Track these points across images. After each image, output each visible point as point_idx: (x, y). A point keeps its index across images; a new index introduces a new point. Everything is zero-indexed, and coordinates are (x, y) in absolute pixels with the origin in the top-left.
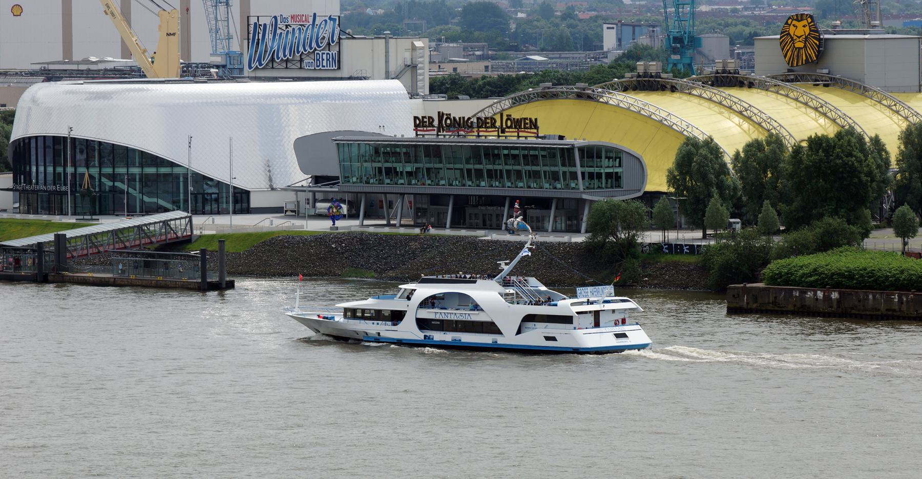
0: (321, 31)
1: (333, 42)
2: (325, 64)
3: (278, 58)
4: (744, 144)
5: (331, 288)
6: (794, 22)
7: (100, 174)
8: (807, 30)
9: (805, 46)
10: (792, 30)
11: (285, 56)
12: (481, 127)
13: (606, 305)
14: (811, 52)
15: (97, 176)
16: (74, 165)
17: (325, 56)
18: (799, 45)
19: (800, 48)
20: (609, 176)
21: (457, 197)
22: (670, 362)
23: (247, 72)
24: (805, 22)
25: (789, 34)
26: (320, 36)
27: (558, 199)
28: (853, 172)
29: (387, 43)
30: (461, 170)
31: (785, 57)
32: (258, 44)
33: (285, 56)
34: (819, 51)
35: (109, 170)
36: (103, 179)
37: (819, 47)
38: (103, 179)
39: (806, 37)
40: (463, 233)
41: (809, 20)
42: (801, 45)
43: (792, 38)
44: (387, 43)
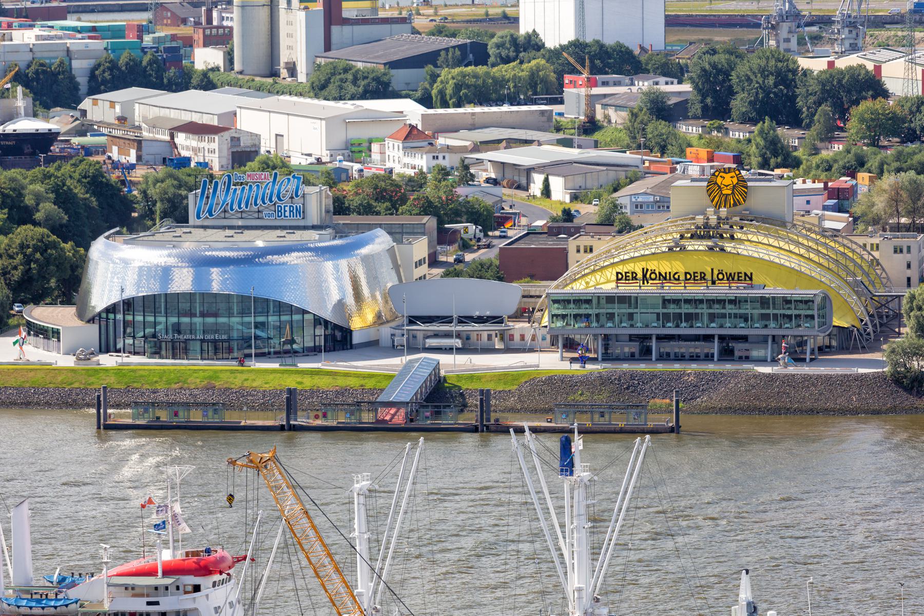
0: (283, 187)
1: (297, 196)
2: (287, 214)
3: (232, 209)
5: (143, 440)
6: (722, 174)
8: (735, 180)
9: (733, 193)
10: (719, 180)
11: (240, 207)
17: (287, 209)
18: (726, 191)
19: (727, 195)
20: (807, 316)
22: (643, 463)
23: (192, 219)
26: (283, 192)
28: (131, 231)
30: (658, 314)
31: (712, 201)
32: (208, 197)
33: (240, 207)
39: (734, 187)
42: (730, 192)
43: (719, 187)
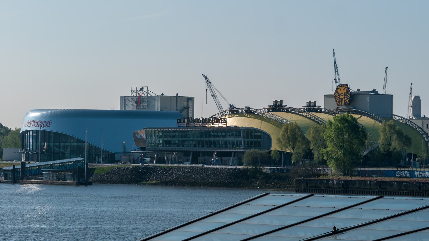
4: (162, 85)
6: (340, 88)
7: (54, 146)
9: (344, 97)
10: (339, 91)
12: (179, 122)
13: (426, 126)
14: (346, 100)
15: (53, 146)
16: (71, 143)
18: (342, 97)
19: (342, 98)
21: (194, 152)
24: (344, 88)
25: (338, 93)
27: (235, 152)
29: (220, 108)
34: (350, 100)
35: (57, 144)
36: (55, 148)
37: (350, 98)
38: (55, 148)
39: (345, 94)
40: (194, 165)
41: (346, 87)
42: (343, 97)
44: (220, 108)
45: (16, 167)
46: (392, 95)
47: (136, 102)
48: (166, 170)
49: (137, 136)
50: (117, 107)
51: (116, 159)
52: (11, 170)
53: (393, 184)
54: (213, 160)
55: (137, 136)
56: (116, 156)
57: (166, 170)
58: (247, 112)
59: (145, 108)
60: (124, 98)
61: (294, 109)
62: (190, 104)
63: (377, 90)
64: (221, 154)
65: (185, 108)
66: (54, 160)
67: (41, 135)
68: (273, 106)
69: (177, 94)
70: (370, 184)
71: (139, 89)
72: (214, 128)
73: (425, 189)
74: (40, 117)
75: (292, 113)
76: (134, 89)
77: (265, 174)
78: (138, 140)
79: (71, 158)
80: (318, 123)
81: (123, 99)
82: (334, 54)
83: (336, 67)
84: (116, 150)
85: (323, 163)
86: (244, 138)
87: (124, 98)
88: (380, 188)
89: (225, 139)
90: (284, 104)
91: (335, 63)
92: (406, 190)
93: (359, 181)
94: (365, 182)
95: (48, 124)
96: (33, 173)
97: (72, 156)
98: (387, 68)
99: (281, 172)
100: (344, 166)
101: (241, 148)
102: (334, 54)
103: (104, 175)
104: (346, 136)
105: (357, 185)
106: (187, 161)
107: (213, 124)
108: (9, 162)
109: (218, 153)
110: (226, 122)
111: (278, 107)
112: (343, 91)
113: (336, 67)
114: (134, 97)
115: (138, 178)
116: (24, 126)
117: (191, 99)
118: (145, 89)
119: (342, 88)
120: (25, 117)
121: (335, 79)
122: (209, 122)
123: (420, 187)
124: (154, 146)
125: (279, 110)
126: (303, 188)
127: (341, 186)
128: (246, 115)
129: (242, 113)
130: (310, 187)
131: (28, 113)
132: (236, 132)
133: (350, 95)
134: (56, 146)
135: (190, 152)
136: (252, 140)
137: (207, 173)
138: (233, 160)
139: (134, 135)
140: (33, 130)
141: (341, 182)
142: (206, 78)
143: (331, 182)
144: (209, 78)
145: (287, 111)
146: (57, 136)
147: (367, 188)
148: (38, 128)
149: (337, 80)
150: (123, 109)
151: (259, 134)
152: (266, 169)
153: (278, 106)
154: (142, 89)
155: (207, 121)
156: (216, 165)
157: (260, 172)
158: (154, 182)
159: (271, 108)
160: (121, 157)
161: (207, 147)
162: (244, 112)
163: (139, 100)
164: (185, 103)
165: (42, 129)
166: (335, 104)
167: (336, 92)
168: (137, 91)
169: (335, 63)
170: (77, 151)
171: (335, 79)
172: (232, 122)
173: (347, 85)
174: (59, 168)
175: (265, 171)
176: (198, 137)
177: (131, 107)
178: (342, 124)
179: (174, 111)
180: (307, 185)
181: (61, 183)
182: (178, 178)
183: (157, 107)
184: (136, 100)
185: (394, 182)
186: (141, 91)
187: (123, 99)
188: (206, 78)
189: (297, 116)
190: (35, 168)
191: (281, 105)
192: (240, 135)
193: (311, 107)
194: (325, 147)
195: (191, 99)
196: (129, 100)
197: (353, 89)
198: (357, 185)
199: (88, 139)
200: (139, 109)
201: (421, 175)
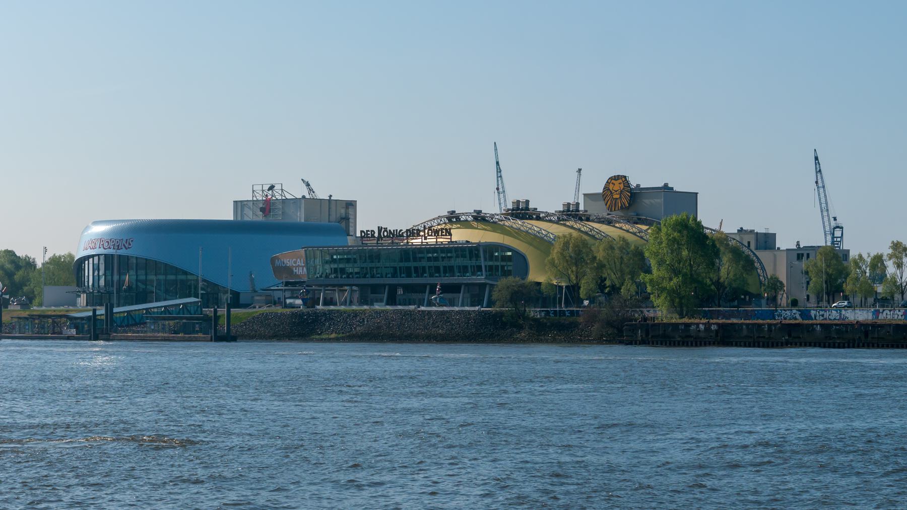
7: (137, 281)
14: (624, 201)
21: (390, 285)
24: (620, 181)
27: (467, 285)
36: (139, 284)
38: (139, 284)
42: (618, 196)
45: (98, 313)
46: (697, 194)
47: (262, 210)
48: (349, 315)
49: (277, 263)
50: (228, 215)
51: (242, 301)
52: (89, 318)
53: (814, 330)
54: (436, 299)
55: (277, 263)
56: (241, 296)
57: (349, 315)
58: (476, 218)
59: (277, 218)
60: (239, 204)
61: (548, 214)
62: (351, 211)
63: (670, 186)
64: (446, 289)
65: (342, 219)
66: (137, 304)
67: (115, 263)
68: (513, 210)
69: (331, 196)
70: (770, 330)
71: (266, 188)
72: (413, 245)
73: (876, 336)
74: (114, 232)
75: (546, 221)
76: (258, 188)
77: (535, 320)
78: (281, 270)
79: (165, 300)
80: (593, 237)
81: (239, 205)
82: (496, 150)
83: (499, 171)
84: (242, 287)
85: (644, 298)
86: (485, 260)
87: (239, 204)
88: (790, 335)
89: (436, 264)
90: (531, 206)
91: (498, 163)
92: (838, 338)
93: (747, 325)
94: (760, 325)
95: (127, 244)
96: (137, 320)
97: (168, 297)
98: (580, 170)
99: (560, 316)
100: (678, 302)
101: (481, 279)
102: (496, 150)
103: (242, 326)
104: (685, 253)
105: (745, 332)
106: (381, 301)
107: (426, 238)
108: (62, 308)
109: (442, 285)
110: (450, 235)
111: (522, 211)
112: (618, 186)
113: (499, 171)
114: (257, 200)
115: (303, 328)
116: (82, 247)
117: (351, 205)
118: (277, 187)
119: (616, 183)
120: (83, 232)
121: (498, 189)
122: (418, 235)
123: (866, 334)
124: (321, 276)
125: (523, 217)
126: (640, 338)
127: (713, 334)
128: (475, 224)
129: (467, 220)
130: (652, 337)
131: (87, 228)
132: (470, 251)
133: (631, 193)
134: (141, 281)
135: (384, 285)
136: (498, 264)
137: (429, 319)
138: (463, 298)
139: (273, 261)
140: (98, 255)
141: (714, 327)
142: (308, 185)
143: (693, 327)
144: (312, 186)
145: (538, 218)
146: (146, 265)
147: (764, 337)
148: (111, 251)
149: (501, 190)
150: (239, 219)
151: (509, 254)
152: (534, 312)
153: (522, 209)
154: (272, 188)
155: (413, 233)
156: (442, 306)
157: (523, 316)
158: (333, 336)
159: (508, 214)
160: (253, 297)
161: (418, 276)
162: (470, 218)
163: (267, 206)
164: (343, 211)
165: (120, 252)
166: (605, 208)
167: (606, 188)
168: (263, 191)
169: (498, 163)
170: (187, 289)
171: (498, 189)
172: (459, 235)
173: (625, 177)
174: (179, 313)
175: (532, 314)
176: (401, 261)
177: (251, 216)
178: (680, 232)
179: (325, 221)
180: (647, 334)
181: (183, 337)
182: (379, 328)
183: (300, 217)
184: (261, 205)
185: (817, 324)
186: (270, 192)
187: (239, 205)
188: (308, 185)
189: (555, 226)
190: (122, 315)
191: (527, 209)
192: (478, 256)
193: (570, 213)
194: (648, 271)
195: (351, 205)
196: (249, 208)
197: (633, 183)
198: (745, 332)
199: (201, 269)
200: (265, 222)
201: (823, 316)
